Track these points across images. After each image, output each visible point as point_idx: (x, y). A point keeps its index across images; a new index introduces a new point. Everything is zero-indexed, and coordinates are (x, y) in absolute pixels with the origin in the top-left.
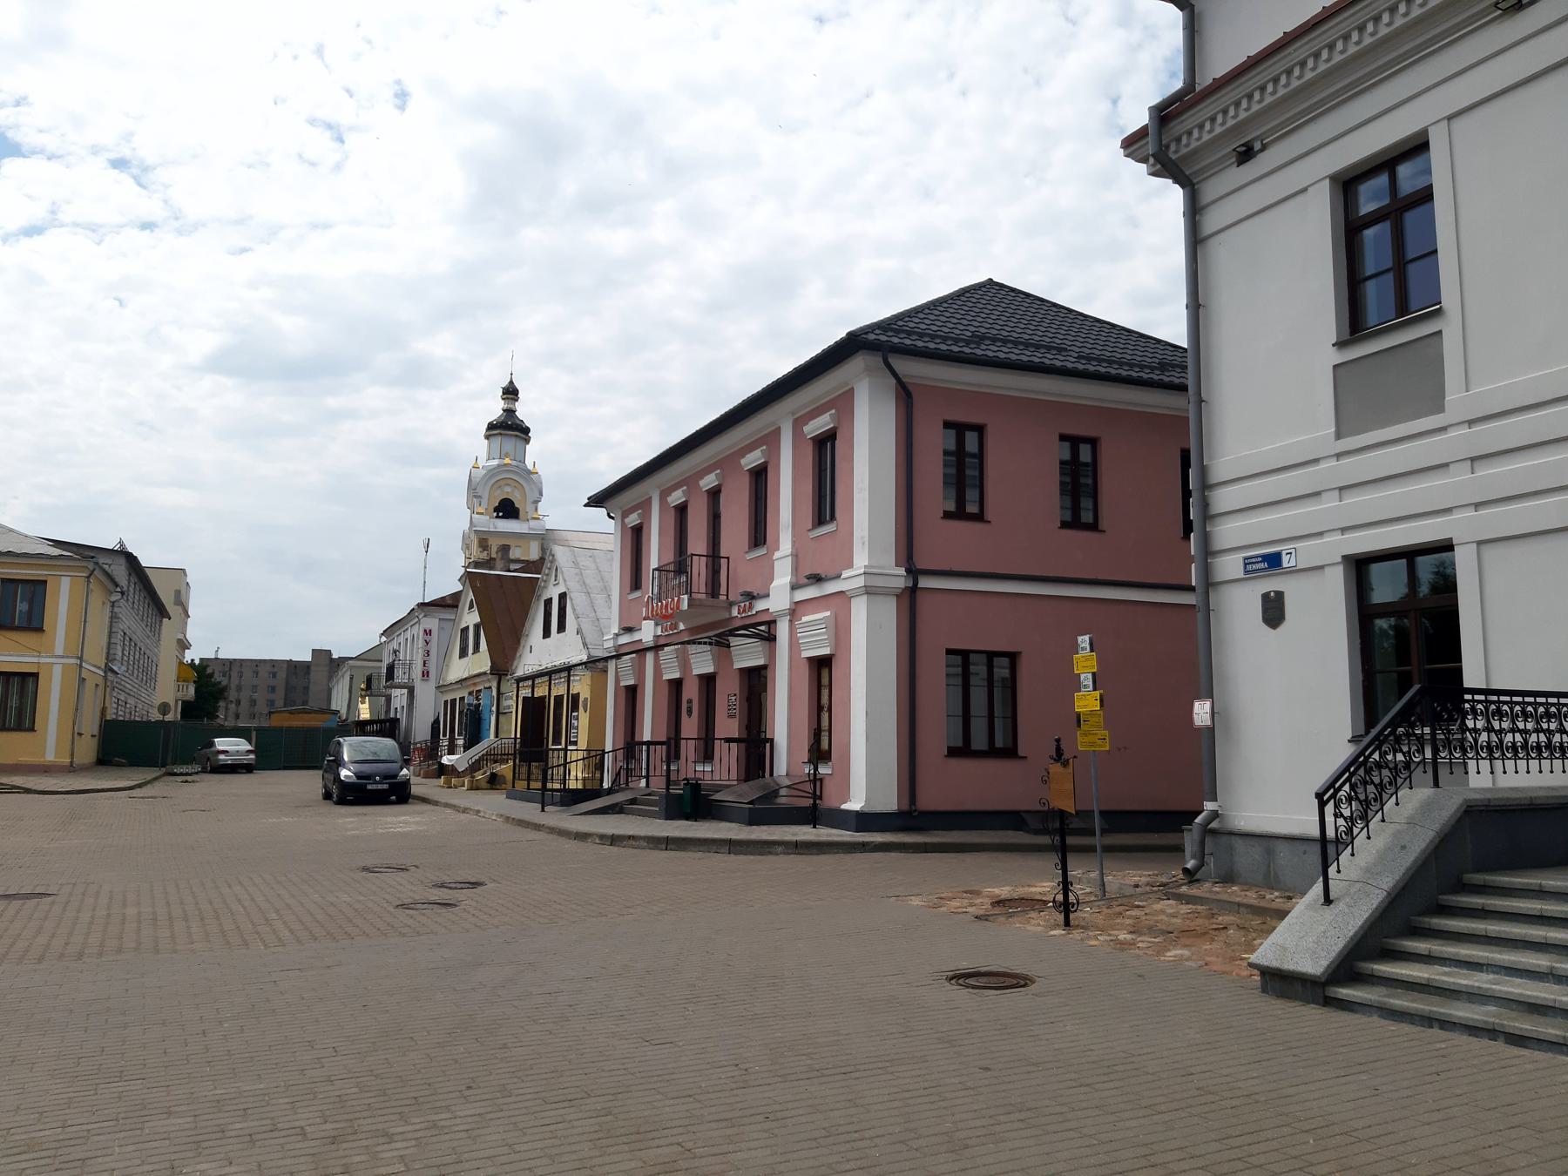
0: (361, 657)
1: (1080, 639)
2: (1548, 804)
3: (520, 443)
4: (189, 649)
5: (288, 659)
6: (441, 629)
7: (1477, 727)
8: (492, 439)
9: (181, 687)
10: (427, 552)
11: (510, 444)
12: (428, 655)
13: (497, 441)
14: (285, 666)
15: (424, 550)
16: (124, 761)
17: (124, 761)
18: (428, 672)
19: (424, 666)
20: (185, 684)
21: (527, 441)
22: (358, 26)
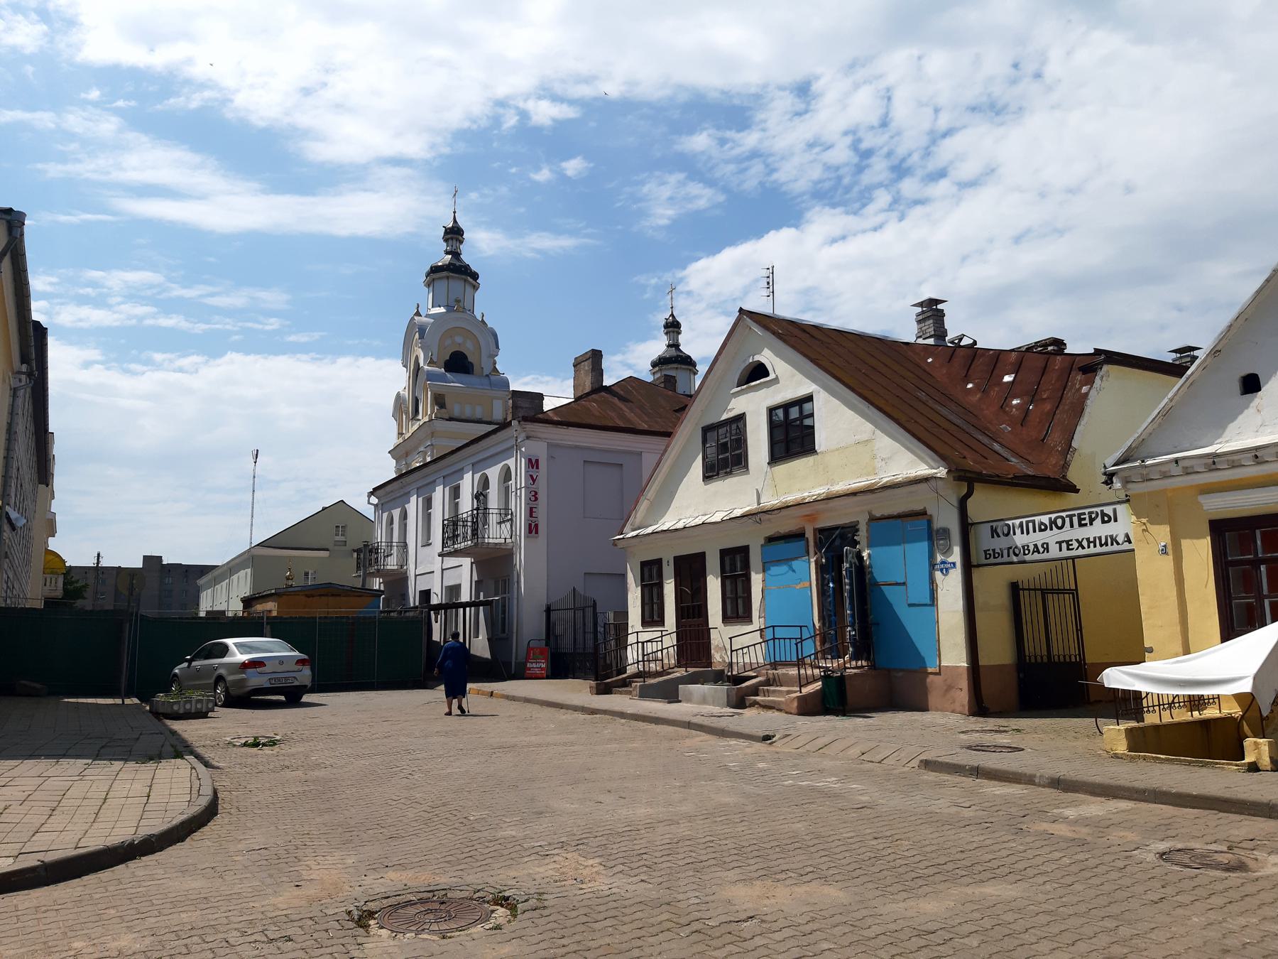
0: (263, 544)
1: (276, 614)
2: (649, 700)
3: (469, 289)
4: (435, 270)
5: (117, 566)
6: (551, 457)
7: (805, 659)
8: (437, 284)
9: (48, 580)
10: (255, 462)
11: (457, 285)
12: (536, 499)
13: (442, 285)
14: (115, 572)
15: (253, 461)
16: (38, 686)
17: (38, 686)
18: (536, 526)
19: (531, 516)
20: (56, 576)
21: (476, 288)
22: (211, 65)
